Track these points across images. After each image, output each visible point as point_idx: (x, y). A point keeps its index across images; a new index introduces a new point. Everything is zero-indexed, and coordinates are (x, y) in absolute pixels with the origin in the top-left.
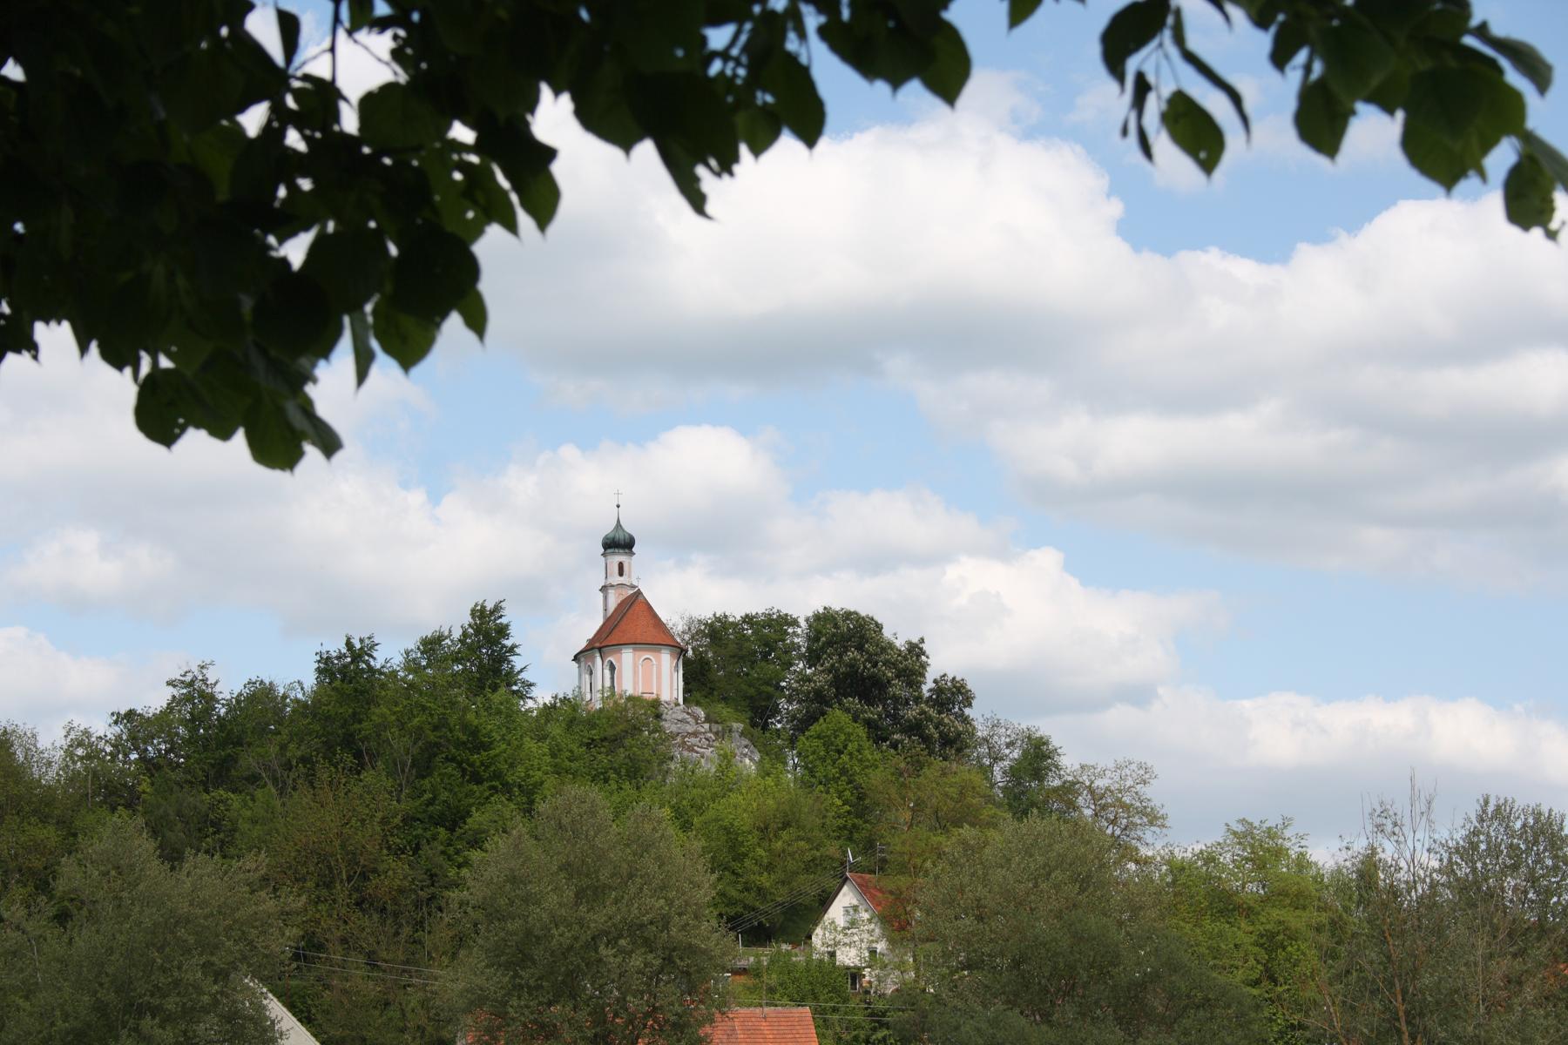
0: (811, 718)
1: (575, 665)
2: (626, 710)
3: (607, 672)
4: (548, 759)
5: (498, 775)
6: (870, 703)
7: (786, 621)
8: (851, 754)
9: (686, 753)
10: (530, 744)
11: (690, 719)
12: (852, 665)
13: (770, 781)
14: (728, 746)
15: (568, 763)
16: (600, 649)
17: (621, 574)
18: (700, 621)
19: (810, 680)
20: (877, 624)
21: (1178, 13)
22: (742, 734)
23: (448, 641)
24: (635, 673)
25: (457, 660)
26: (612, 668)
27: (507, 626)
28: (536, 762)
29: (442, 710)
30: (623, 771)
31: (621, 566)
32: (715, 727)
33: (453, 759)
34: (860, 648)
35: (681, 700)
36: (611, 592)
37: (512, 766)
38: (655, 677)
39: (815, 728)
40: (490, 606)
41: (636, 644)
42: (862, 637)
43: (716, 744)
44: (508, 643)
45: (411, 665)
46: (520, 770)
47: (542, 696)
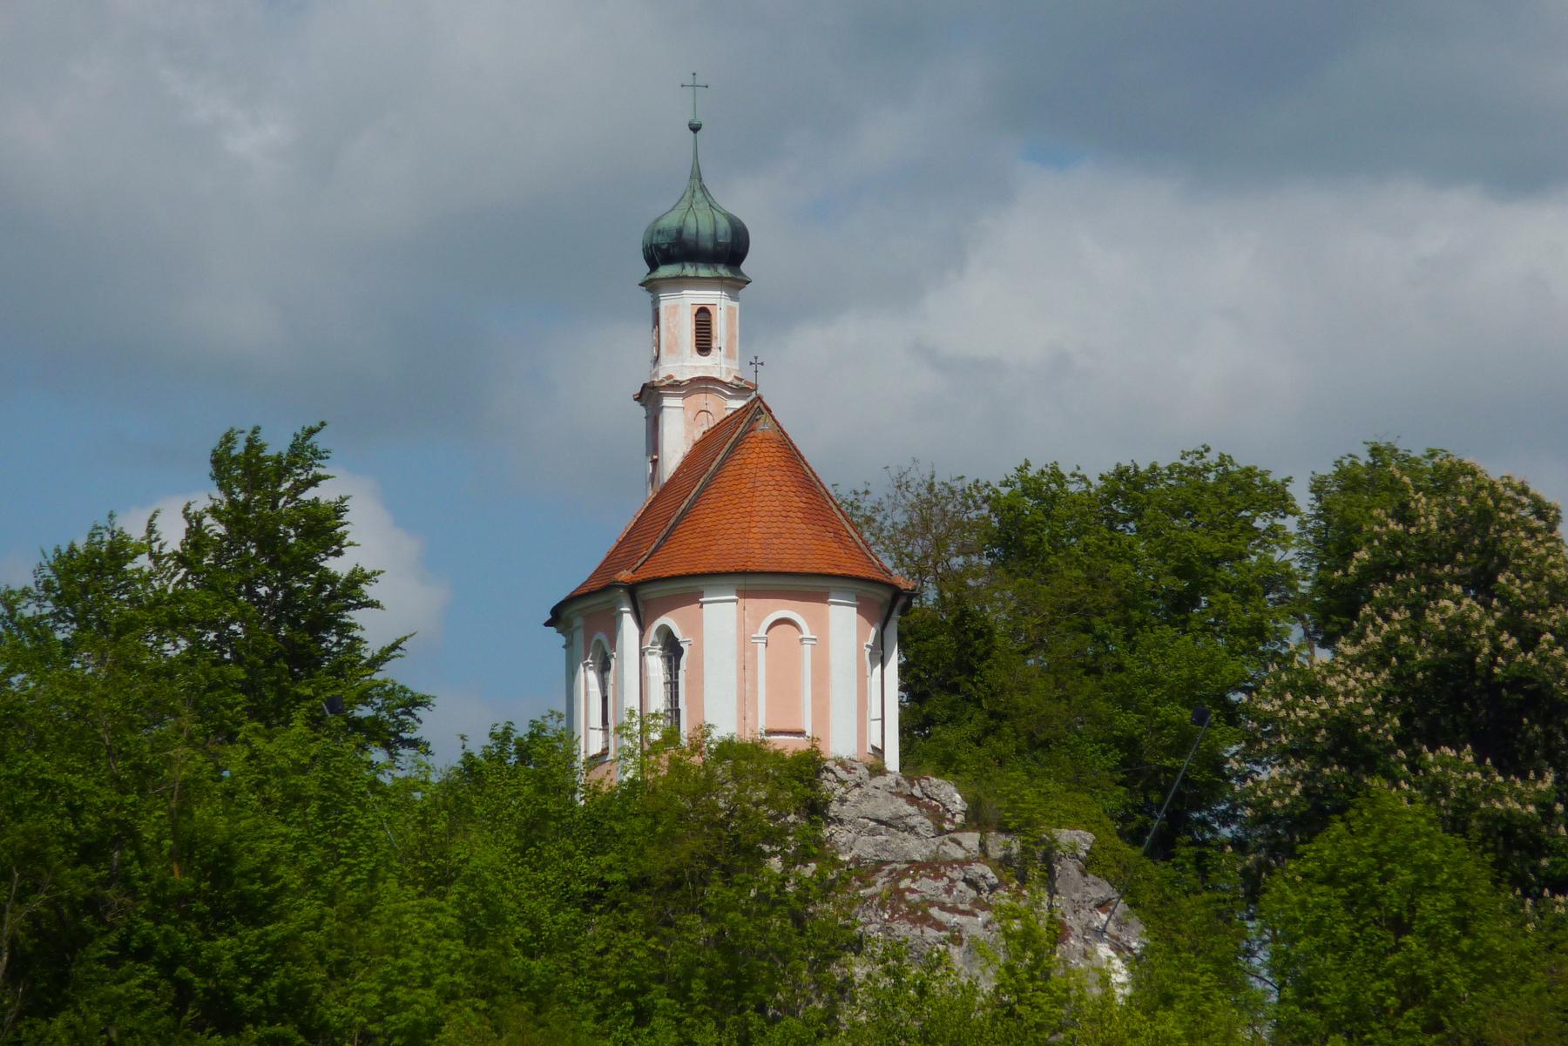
0: (1314, 815)
1: (555, 638)
2: (708, 785)
3: (656, 664)
4: (455, 948)
6: (1513, 762)
7: (1240, 494)
8: (1430, 934)
9: (902, 929)
10: (399, 900)
11: (918, 819)
12: (1456, 638)
15: (519, 959)
16: (633, 590)
17: (704, 344)
19: (1314, 689)
20: (1541, 509)
21: (770, 733)
22: (1089, 864)
23: (144, 562)
24: (745, 667)
25: (175, 624)
26: (672, 649)
27: (338, 510)
28: (414, 960)
29: (109, 794)
30: (698, 986)
31: (703, 319)
32: (998, 845)
34: (1482, 585)
35: (892, 760)
36: (672, 405)
37: (340, 970)
38: (799, 679)
39: (1324, 848)
40: (277, 444)
41: (755, 581)
42: (1488, 549)
43: (1003, 898)
44: (338, 566)
46: (367, 988)
47: (452, 730)
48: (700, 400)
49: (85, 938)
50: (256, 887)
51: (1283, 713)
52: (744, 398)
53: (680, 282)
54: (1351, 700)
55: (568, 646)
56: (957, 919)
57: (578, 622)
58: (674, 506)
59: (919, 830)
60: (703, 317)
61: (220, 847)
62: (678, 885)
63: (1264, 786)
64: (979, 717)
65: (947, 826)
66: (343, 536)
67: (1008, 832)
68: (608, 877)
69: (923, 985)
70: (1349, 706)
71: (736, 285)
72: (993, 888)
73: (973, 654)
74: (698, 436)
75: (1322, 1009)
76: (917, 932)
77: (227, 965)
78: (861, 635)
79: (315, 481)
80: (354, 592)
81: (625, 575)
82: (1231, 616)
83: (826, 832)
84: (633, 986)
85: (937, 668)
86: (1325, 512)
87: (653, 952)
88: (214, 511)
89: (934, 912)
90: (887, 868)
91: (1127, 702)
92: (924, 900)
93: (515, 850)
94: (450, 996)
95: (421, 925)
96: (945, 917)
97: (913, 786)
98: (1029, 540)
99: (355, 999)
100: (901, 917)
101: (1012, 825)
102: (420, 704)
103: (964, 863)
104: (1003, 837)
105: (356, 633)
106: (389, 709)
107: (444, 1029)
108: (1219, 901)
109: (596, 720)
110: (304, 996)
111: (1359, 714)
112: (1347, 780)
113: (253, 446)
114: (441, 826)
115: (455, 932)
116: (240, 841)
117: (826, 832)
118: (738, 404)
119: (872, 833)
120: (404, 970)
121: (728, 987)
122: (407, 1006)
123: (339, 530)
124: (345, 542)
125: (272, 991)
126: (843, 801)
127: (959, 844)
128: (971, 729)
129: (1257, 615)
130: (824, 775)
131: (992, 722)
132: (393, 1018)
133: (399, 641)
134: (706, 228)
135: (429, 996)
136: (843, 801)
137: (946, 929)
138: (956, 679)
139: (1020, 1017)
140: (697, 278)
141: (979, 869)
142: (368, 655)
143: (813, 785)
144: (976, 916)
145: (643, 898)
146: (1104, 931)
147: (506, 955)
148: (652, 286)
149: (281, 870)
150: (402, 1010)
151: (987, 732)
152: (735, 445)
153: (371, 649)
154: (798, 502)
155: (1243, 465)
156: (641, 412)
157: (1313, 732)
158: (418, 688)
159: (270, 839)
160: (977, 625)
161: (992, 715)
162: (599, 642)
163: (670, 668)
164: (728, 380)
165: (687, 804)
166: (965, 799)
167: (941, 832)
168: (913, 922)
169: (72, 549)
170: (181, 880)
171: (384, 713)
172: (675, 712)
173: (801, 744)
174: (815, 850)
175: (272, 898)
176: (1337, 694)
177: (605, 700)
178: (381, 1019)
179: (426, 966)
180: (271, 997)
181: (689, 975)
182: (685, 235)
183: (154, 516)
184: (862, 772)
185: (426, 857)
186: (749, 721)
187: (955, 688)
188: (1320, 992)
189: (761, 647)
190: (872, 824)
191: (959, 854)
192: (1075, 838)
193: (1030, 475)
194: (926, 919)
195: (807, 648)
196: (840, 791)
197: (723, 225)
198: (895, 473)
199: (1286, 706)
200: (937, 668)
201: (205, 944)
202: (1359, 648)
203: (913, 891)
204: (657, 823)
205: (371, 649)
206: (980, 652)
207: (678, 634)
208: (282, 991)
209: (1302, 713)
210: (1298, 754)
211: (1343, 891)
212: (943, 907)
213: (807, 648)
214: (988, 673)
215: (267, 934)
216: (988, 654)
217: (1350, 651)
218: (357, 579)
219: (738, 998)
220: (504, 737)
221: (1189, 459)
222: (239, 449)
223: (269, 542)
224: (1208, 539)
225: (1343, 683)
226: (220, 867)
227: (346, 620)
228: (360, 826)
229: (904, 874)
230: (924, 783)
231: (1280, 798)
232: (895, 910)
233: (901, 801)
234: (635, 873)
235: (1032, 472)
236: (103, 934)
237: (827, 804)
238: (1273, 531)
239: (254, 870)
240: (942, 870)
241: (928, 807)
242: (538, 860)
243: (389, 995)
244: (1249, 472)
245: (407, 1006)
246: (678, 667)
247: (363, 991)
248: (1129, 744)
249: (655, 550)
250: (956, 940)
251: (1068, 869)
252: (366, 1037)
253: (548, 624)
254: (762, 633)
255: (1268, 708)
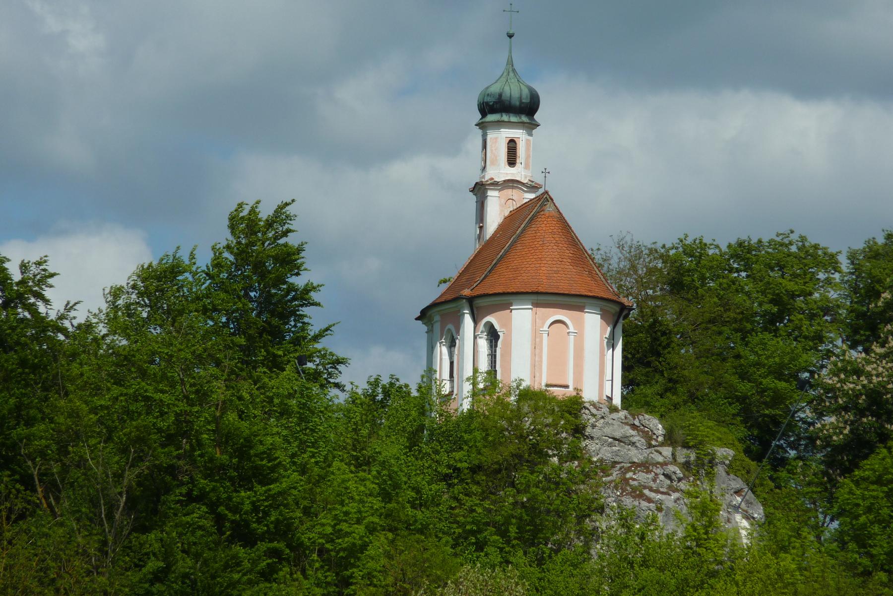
1: (421, 327)
2: (518, 414)
4: (377, 503)
5: (284, 530)
7: (813, 258)
9: (628, 502)
13: (788, 561)
14: (122, 358)
15: (410, 511)
16: (471, 300)
17: (512, 161)
18: (652, 251)
21: (547, 386)
22: (731, 469)
24: (536, 347)
26: (493, 336)
28: (352, 507)
29: (182, 406)
30: (513, 530)
31: (512, 146)
32: (682, 455)
33: (201, 498)
35: (617, 401)
36: (493, 195)
38: (565, 355)
39: (872, 465)
41: (542, 297)
43: (683, 485)
44: (299, 281)
45: (120, 316)
48: (509, 192)
49: (168, 490)
50: (264, 462)
51: (839, 385)
52: (535, 192)
53: (499, 124)
54: (881, 379)
55: (430, 331)
56: (659, 496)
57: (437, 318)
58: (493, 254)
59: (638, 444)
60: (512, 145)
61: (245, 439)
62: (499, 471)
63: (827, 427)
64: (663, 381)
65: (654, 443)
66: (302, 264)
67: (688, 447)
68: (459, 465)
69: (643, 534)
70: (879, 382)
71: (531, 126)
72: (680, 480)
73: (660, 345)
74: (507, 213)
75: (871, 556)
76: (636, 503)
77: (247, 507)
78: (603, 331)
79: (286, 233)
80: (307, 297)
81: (466, 292)
82: (804, 328)
83: (583, 444)
84: (475, 528)
85: (638, 352)
86: (857, 269)
87: (485, 509)
88: (228, 247)
89: (646, 492)
90: (618, 466)
91: (744, 376)
92: (640, 485)
93: (406, 447)
94: (372, 530)
95: (357, 488)
96: (652, 495)
97: (634, 419)
98: (687, 279)
99: (318, 529)
100: (627, 494)
101: (691, 444)
102: (342, 363)
103: (663, 464)
104: (685, 451)
105: (306, 320)
106: (324, 365)
107: (369, 548)
108: (813, 492)
109: (446, 375)
110: (289, 526)
111: (884, 387)
112: (876, 425)
113: (253, 211)
114: (365, 432)
115: (375, 493)
116: (256, 436)
117: (583, 444)
118: (532, 196)
119: (610, 445)
120: (347, 513)
121: (529, 531)
122: (348, 534)
123: (298, 261)
124: (302, 268)
125: (272, 523)
126: (594, 426)
127: (660, 453)
128: (658, 388)
129: (819, 328)
130: (584, 411)
131: (670, 385)
132: (340, 540)
133: (330, 326)
134: (515, 94)
135: (361, 529)
136: (594, 426)
137: (653, 502)
138: (649, 359)
139: (699, 554)
140: (509, 122)
141: (672, 468)
142: (312, 334)
143: (576, 417)
144: (669, 495)
145: (481, 477)
146: (739, 507)
147: (404, 508)
148: (482, 126)
149: (278, 454)
150: (345, 536)
151: (667, 390)
152: (532, 219)
153: (313, 330)
154: (568, 253)
155: (813, 243)
156: (473, 198)
157: (858, 396)
158: (340, 353)
159: (273, 435)
160: (663, 328)
161: (670, 380)
162: (449, 330)
163: (491, 346)
164: (525, 182)
165: (504, 423)
166: (664, 427)
167: (650, 446)
168: (634, 497)
169: (150, 266)
170: (221, 457)
171: (320, 367)
172: (492, 372)
173: (571, 392)
174: (579, 455)
175: (273, 469)
176: (872, 375)
177: (452, 363)
178: (332, 541)
179: (360, 512)
180: (272, 526)
181: (507, 522)
182: (503, 98)
183: (194, 249)
184: (605, 410)
185: (355, 450)
186: (537, 378)
187: (648, 364)
188: (871, 546)
189: (545, 336)
190: (610, 440)
191: (660, 459)
192: (724, 453)
193: (687, 242)
194: (641, 496)
195: (572, 337)
196: (593, 420)
197: (526, 92)
198: (616, 240)
199: (840, 381)
200: (638, 352)
201: (234, 494)
202: (885, 349)
203: (634, 480)
204: (487, 435)
205: (313, 330)
206: (664, 344)
207: (497, 327)
208: (277, 522)
209: (852, 386)
210: (846, 409)
211: (885, 489)
212: (651, 490)
213: (572, 337)
214: (668, 356)
215: (270, 490)
216: (668, 345)
217: (879, 350)
218: (309, 288)
219: (535, 537)
220: (375, 383)
221: (781, 237)
222: (245, 213)
223: (259, 267)
224: (792, 283)
225: (874, 369)
226: (243, 450)
227: (301, 313)
228: (320, 430)
229: (628, 470)
230: (641, 417)
231: (837, 435)
232: (623, 490)
233: (627, 427)
234: (476, 462)
235: (689, 241)
236: (178, 486)
237: (584, 428)
238: (828, 281)
239: (264, 453)
240: (651, 468)
241: (643, 432)
242: (419, 454)
243: (338, 527)
244: (816, 247)
245: (348, 534)
246: (496, 346)
247: (323, 525)
248: (742, 399)
249: (484, 278)
250: (660, 509)
251: (720, 470)
252: (106, 593)
253: (417, 319)
254: (546, 328)
255: (830, 382)
